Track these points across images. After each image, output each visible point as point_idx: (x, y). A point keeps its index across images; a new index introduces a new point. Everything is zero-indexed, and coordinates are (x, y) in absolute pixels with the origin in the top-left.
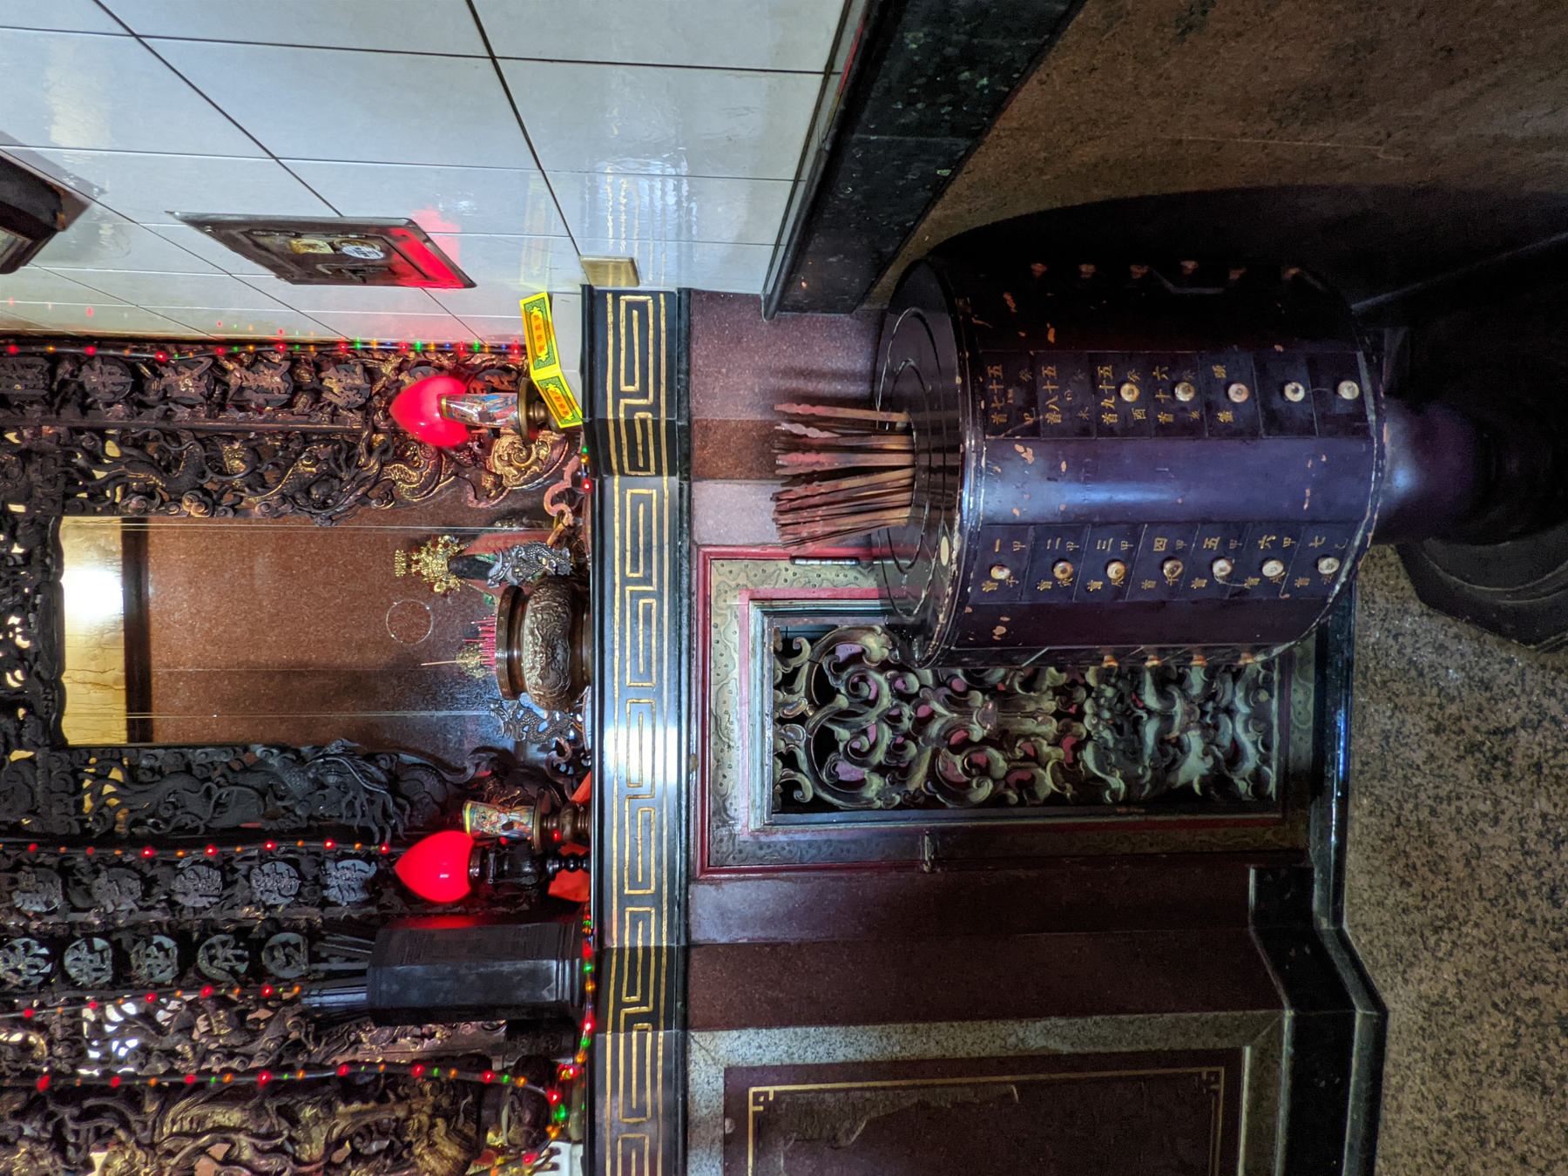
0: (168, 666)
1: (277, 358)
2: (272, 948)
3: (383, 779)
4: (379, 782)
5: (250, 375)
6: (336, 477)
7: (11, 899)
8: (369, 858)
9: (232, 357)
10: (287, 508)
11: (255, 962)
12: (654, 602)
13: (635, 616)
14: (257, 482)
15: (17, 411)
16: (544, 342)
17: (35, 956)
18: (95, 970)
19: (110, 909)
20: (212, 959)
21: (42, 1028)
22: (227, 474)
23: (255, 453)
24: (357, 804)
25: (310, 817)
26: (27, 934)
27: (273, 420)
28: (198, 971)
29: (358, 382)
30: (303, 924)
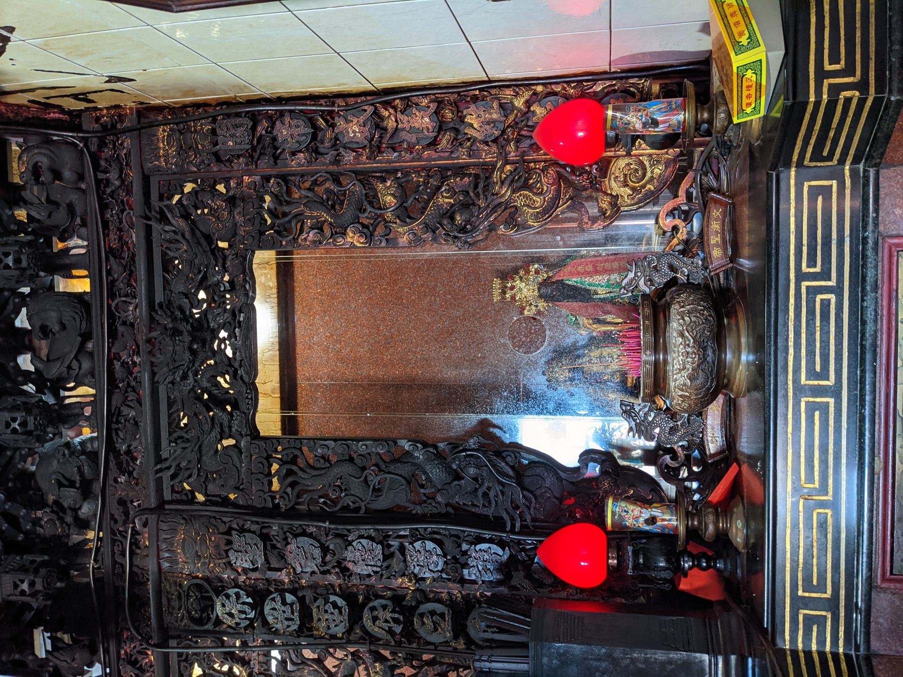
0: (309, 380)
1: (425, 102)
2: (422, 615)
3: (511, 473)
4: (508, 476)
5: (404, 118)
6: (474, 204)
7: (228, 556)
8: (502, 544)
9: (387, 104)
10: (428, 236)
11: (408, 625)
12: (832, 297)
13: (811, 312)
14: (405, 214)
15: (228, 164)
16: (742, 27)
17: (244, 603)
18: (287, 619)
19: (299, 570)
20: (375, 619)
21: (244, 663)
22: (380, 209)
23: (404, 191)
24: (492, 494)
25: (447, 505)
26: (237, 586)
27: (419, 160)
28: (363, 627)
29: (495, 116)
30: (444, 596)
